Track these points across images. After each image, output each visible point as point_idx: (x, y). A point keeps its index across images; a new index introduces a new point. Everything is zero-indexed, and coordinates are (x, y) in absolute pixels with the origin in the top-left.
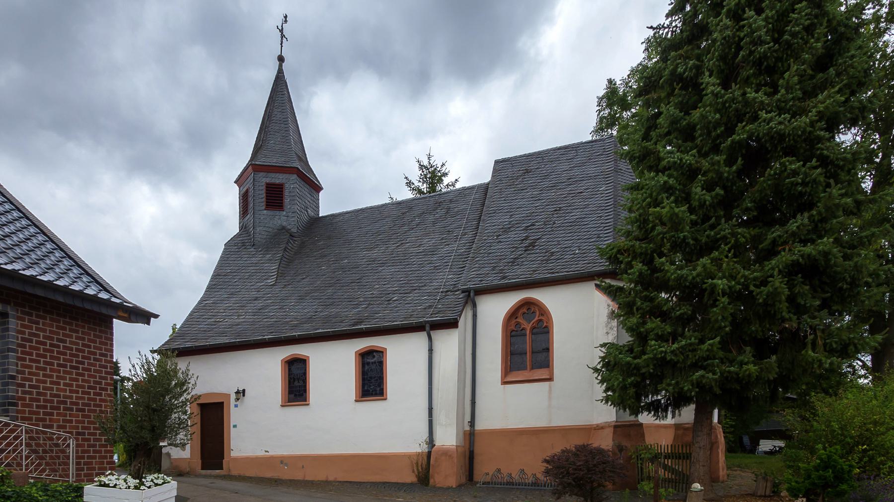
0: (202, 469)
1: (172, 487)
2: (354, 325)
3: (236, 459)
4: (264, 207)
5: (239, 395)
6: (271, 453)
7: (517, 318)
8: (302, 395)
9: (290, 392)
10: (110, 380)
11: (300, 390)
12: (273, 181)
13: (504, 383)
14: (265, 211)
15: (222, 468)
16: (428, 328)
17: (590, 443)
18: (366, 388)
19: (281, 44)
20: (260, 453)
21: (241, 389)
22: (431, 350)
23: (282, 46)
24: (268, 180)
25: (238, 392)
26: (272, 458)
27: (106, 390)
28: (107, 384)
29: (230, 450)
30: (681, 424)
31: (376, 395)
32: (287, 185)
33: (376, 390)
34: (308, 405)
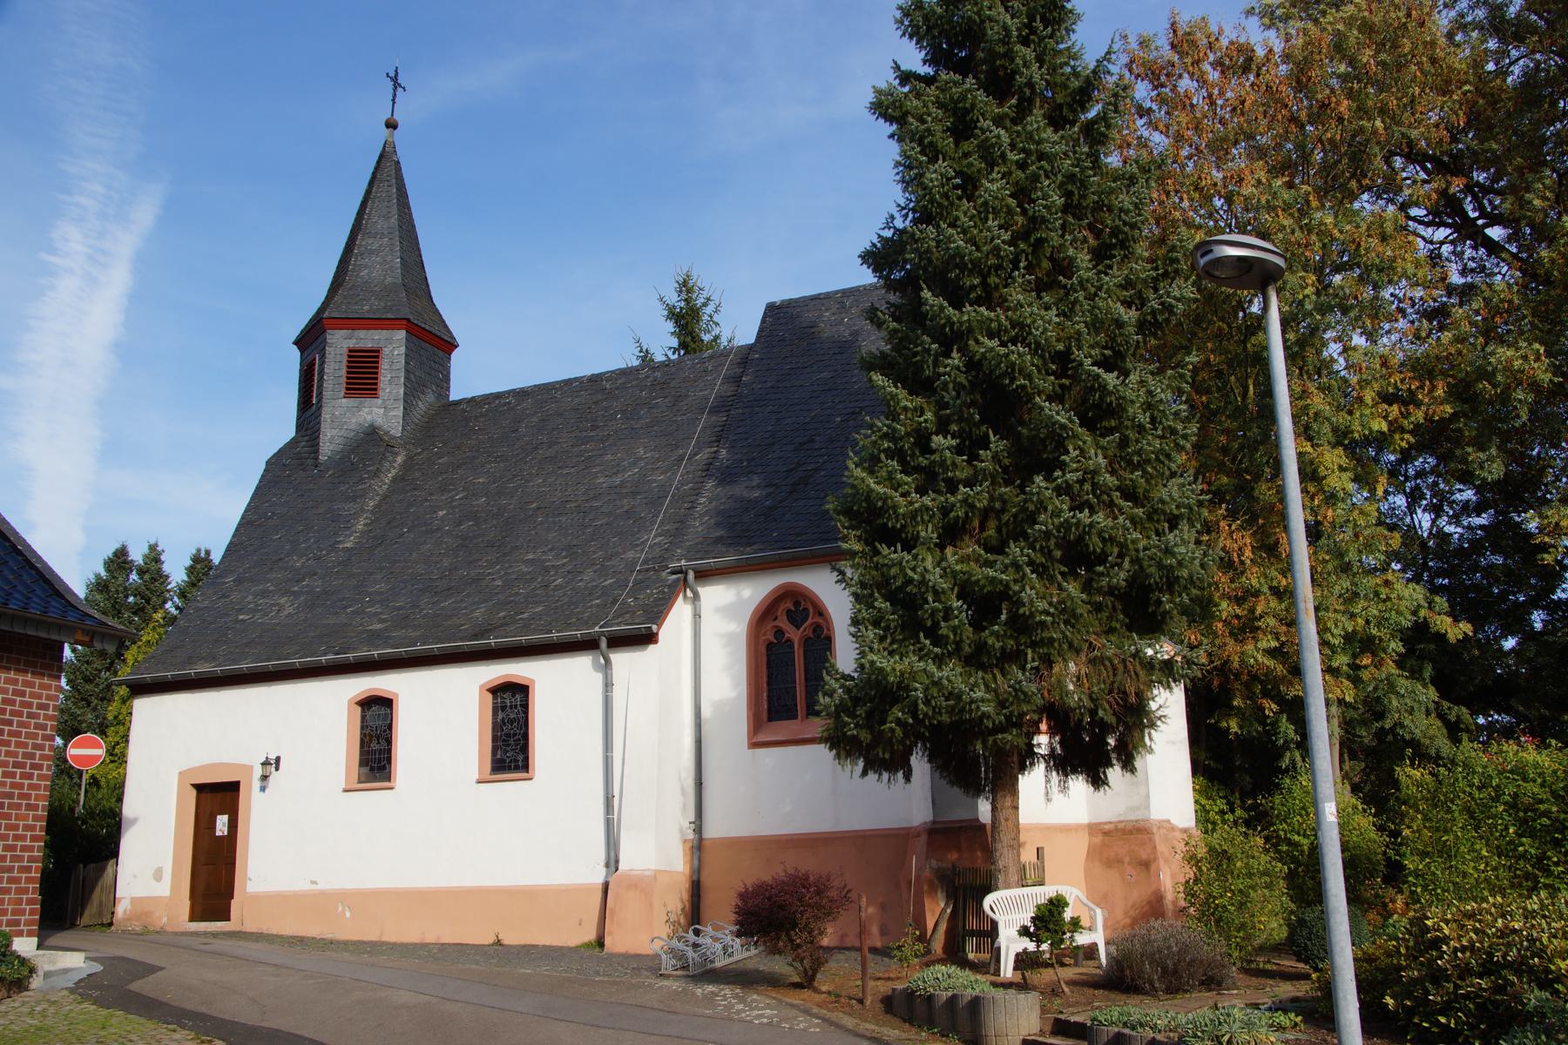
0: (192, 918)
1: (1565, 218)
2: (475, 637)
3: (256, 898)
4: (342, 394)
5: (268, 767)
6: (322, 886)
7: (776, 619)
8: (384, 768)
9: (363, 763)
10: (49, 750)
11: (380, 759)
12: (361, 345)
13: (754, 745)
14: (344, 400)
15: (228, 919)
16: (604, 643)
17: (1181, 847)
18: (499, 757)
19: (393, 100)
20: (302, 885)
21: (273, 756)
22: (608, 685)
23: (394, 103)
24: (352, 344)
25: (266, 763)
26: (323, 894)
27: (40, 767)
28: (43, 757)
29: (245, 878)
30: (1100, 824)
31: (517, 769)
32: (386, 351)
33: (516, 761)
34: (392, 788)
